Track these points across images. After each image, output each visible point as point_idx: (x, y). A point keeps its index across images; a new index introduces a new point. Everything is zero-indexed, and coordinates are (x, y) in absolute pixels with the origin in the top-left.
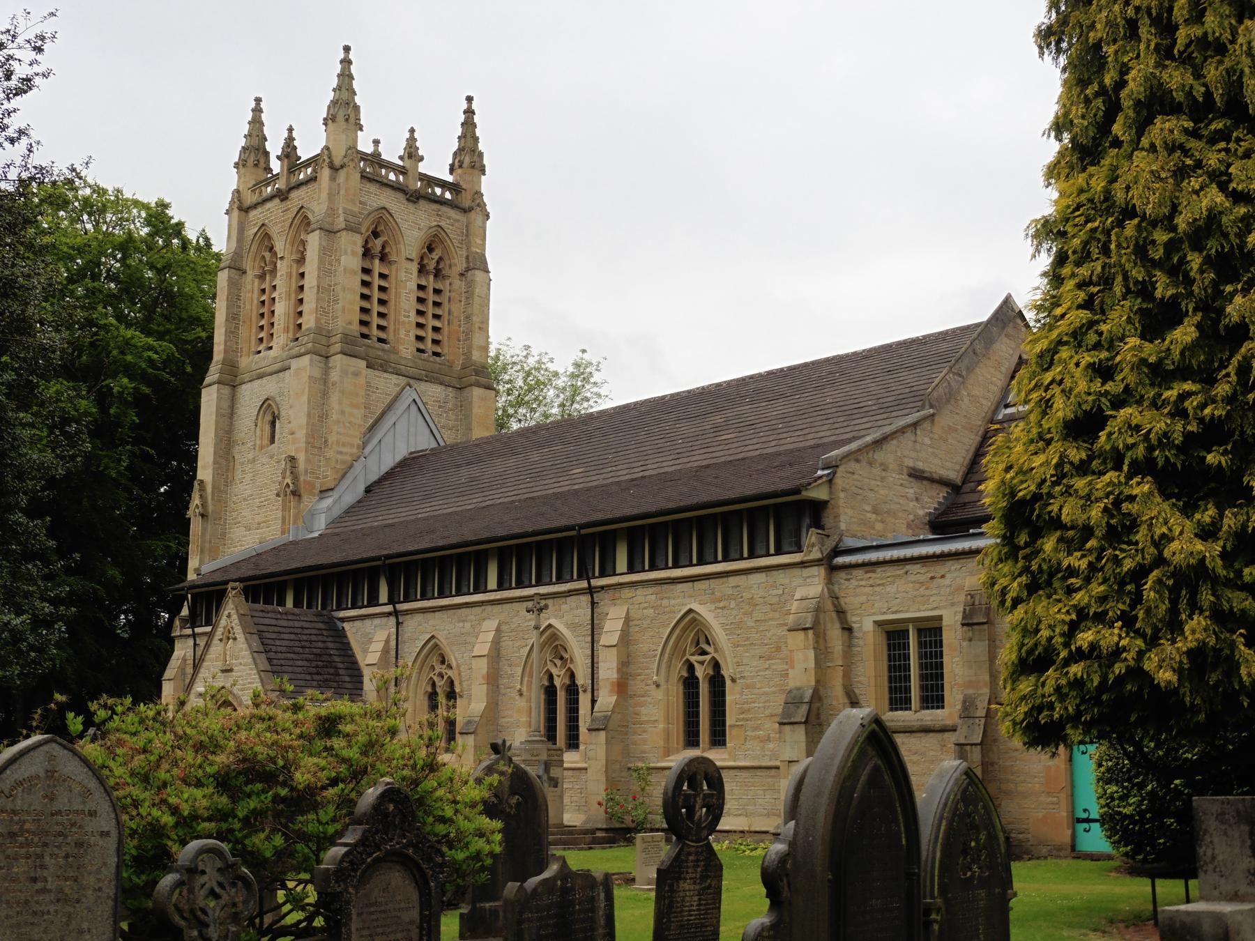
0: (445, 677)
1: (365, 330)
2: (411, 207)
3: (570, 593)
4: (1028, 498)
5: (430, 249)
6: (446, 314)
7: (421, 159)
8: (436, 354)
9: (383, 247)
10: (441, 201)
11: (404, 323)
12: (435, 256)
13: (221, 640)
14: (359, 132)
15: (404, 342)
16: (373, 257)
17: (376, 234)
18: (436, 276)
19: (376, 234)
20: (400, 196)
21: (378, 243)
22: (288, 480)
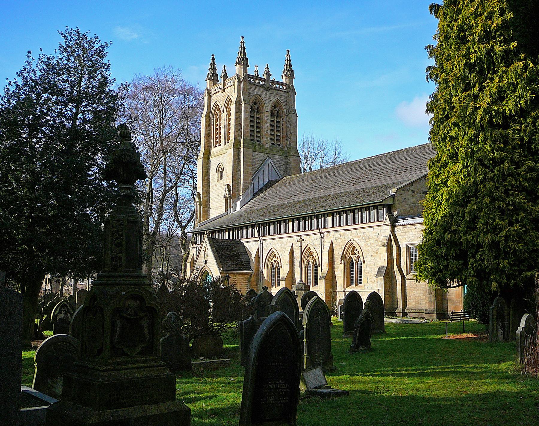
0: (277, 262)
1: (252, 138)
2: (268, 93)
3: (314, 234)
4: (257, 364)
5: (275, 107)
6: (281, 130)
7: (271, 75)
8: (279, 145)
9: (258, 108)
10: (278, 90)
11: (266, 134)
12: (277, 110)
13: (203, 250)
14: (248, 67)
15: (267, 143)
16: (275, 116)
17: (255, 103)
18: (257, 112)
19: (255, 103)
20: (263, 89)
21: (256, 106)
22: (227, 192)
